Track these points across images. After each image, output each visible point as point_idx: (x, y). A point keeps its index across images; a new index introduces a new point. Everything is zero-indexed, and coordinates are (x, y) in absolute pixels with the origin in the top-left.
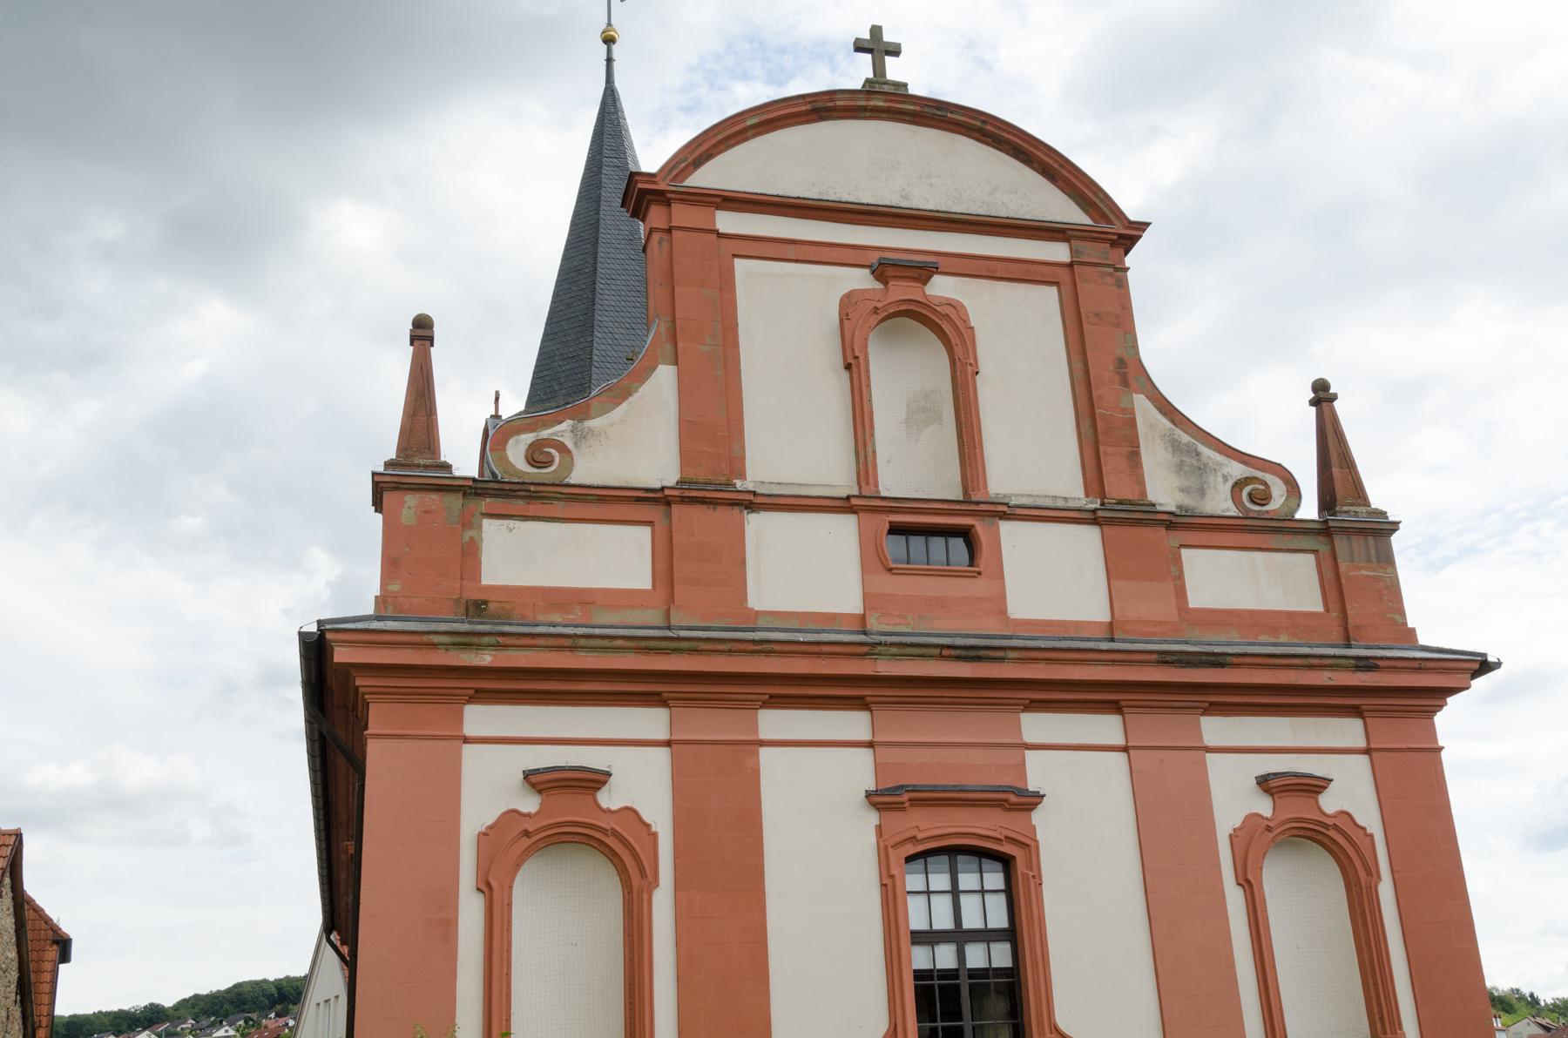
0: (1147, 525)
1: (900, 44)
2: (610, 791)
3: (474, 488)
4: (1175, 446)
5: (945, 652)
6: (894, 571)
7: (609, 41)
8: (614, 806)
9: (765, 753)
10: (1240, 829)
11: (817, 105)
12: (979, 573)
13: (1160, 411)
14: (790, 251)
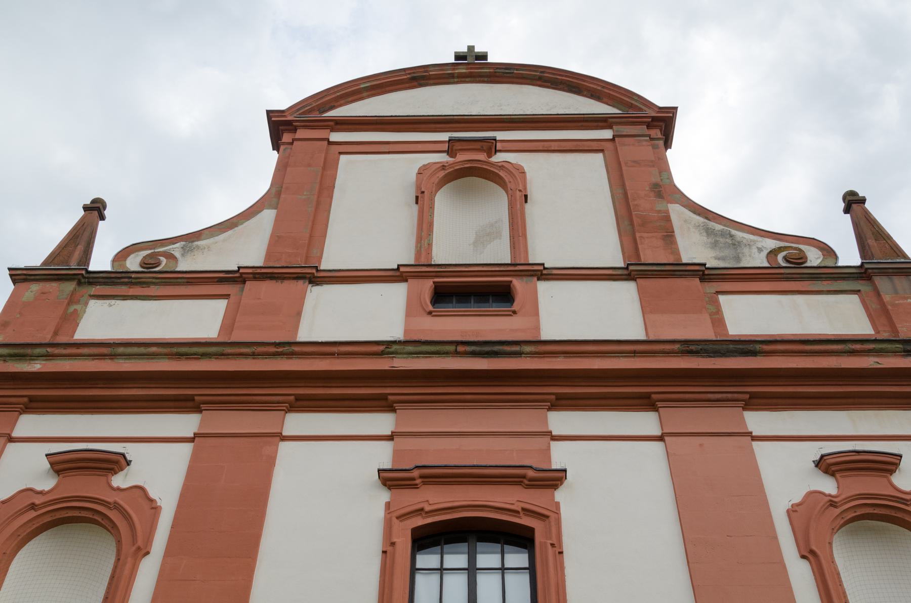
0: (680, 276)
1: (487, 52)
2: (126, 475)
3: (88, 278)
4: (709, 232)
5: (461, 348)
6: (433, 314)
8: (124, 486)
9: (284, 448)
10: (798, 505)
12: (515, 312)
13: (694, 213)
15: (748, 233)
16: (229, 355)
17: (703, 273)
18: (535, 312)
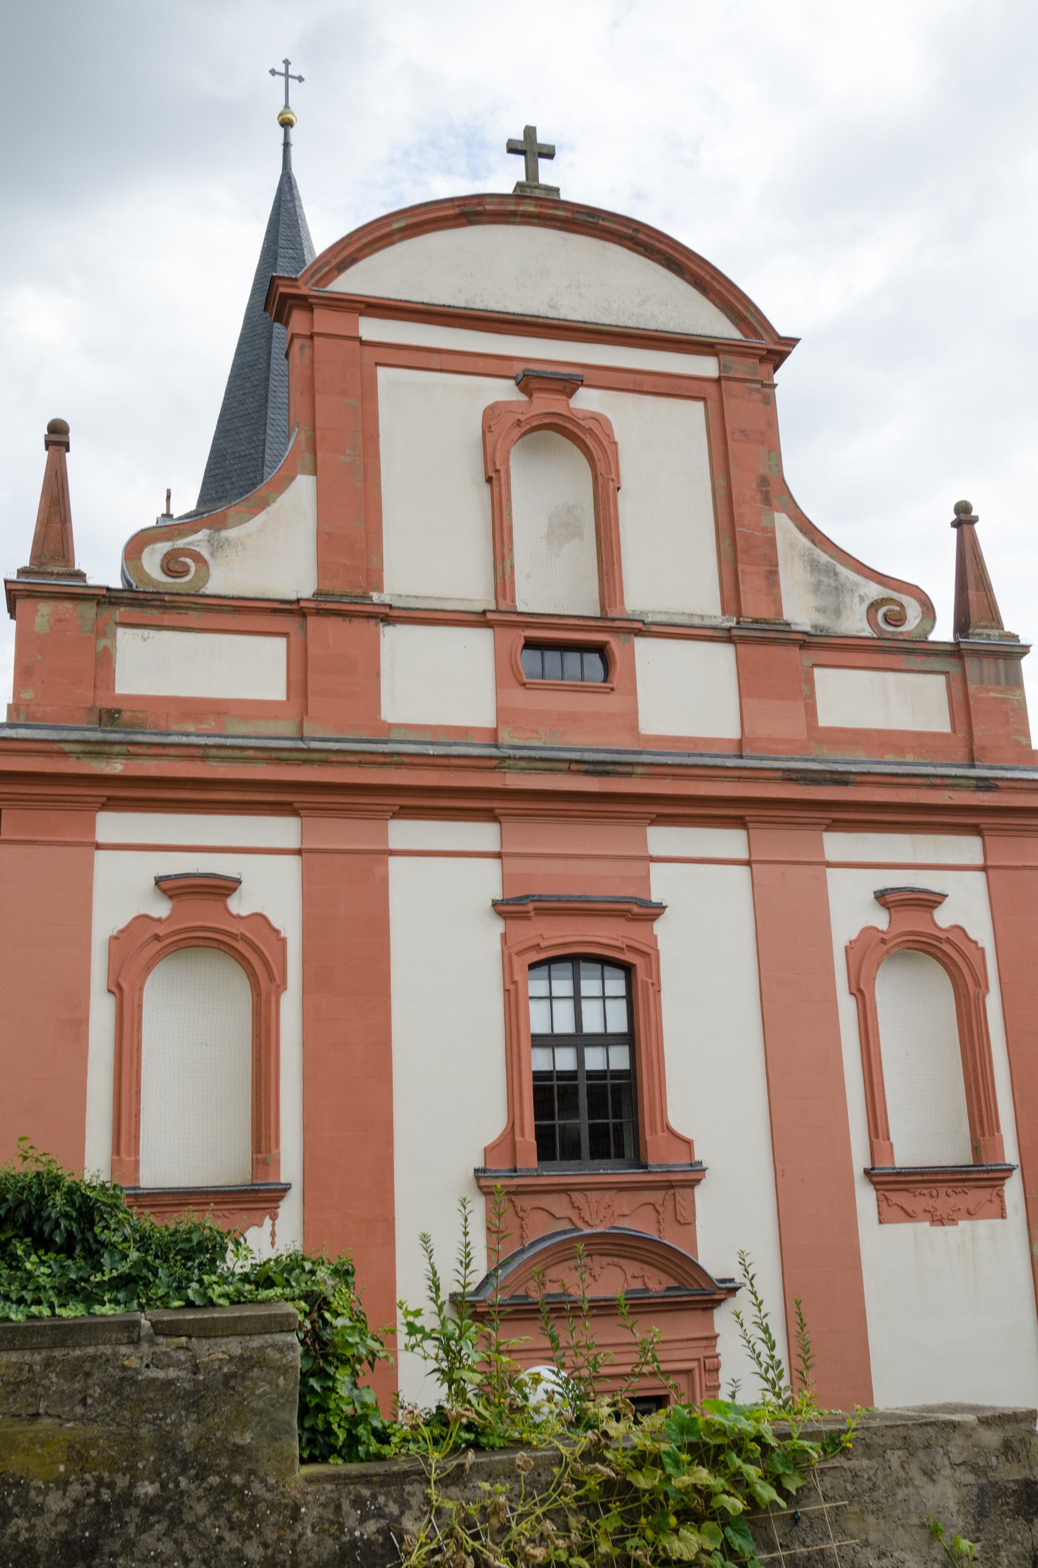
0: (781, 644)
1: (554, 147)
2: (240, 897)
3: (109, 597)
5: (574, 767)
7: (286, 124)
8: (244, 913)
11: (466, 209)
12: (612, 689)
14: (434, 360)
15: (853, 570)
16: (332, 762)
17: (806, 642)
18: (632, 691)
